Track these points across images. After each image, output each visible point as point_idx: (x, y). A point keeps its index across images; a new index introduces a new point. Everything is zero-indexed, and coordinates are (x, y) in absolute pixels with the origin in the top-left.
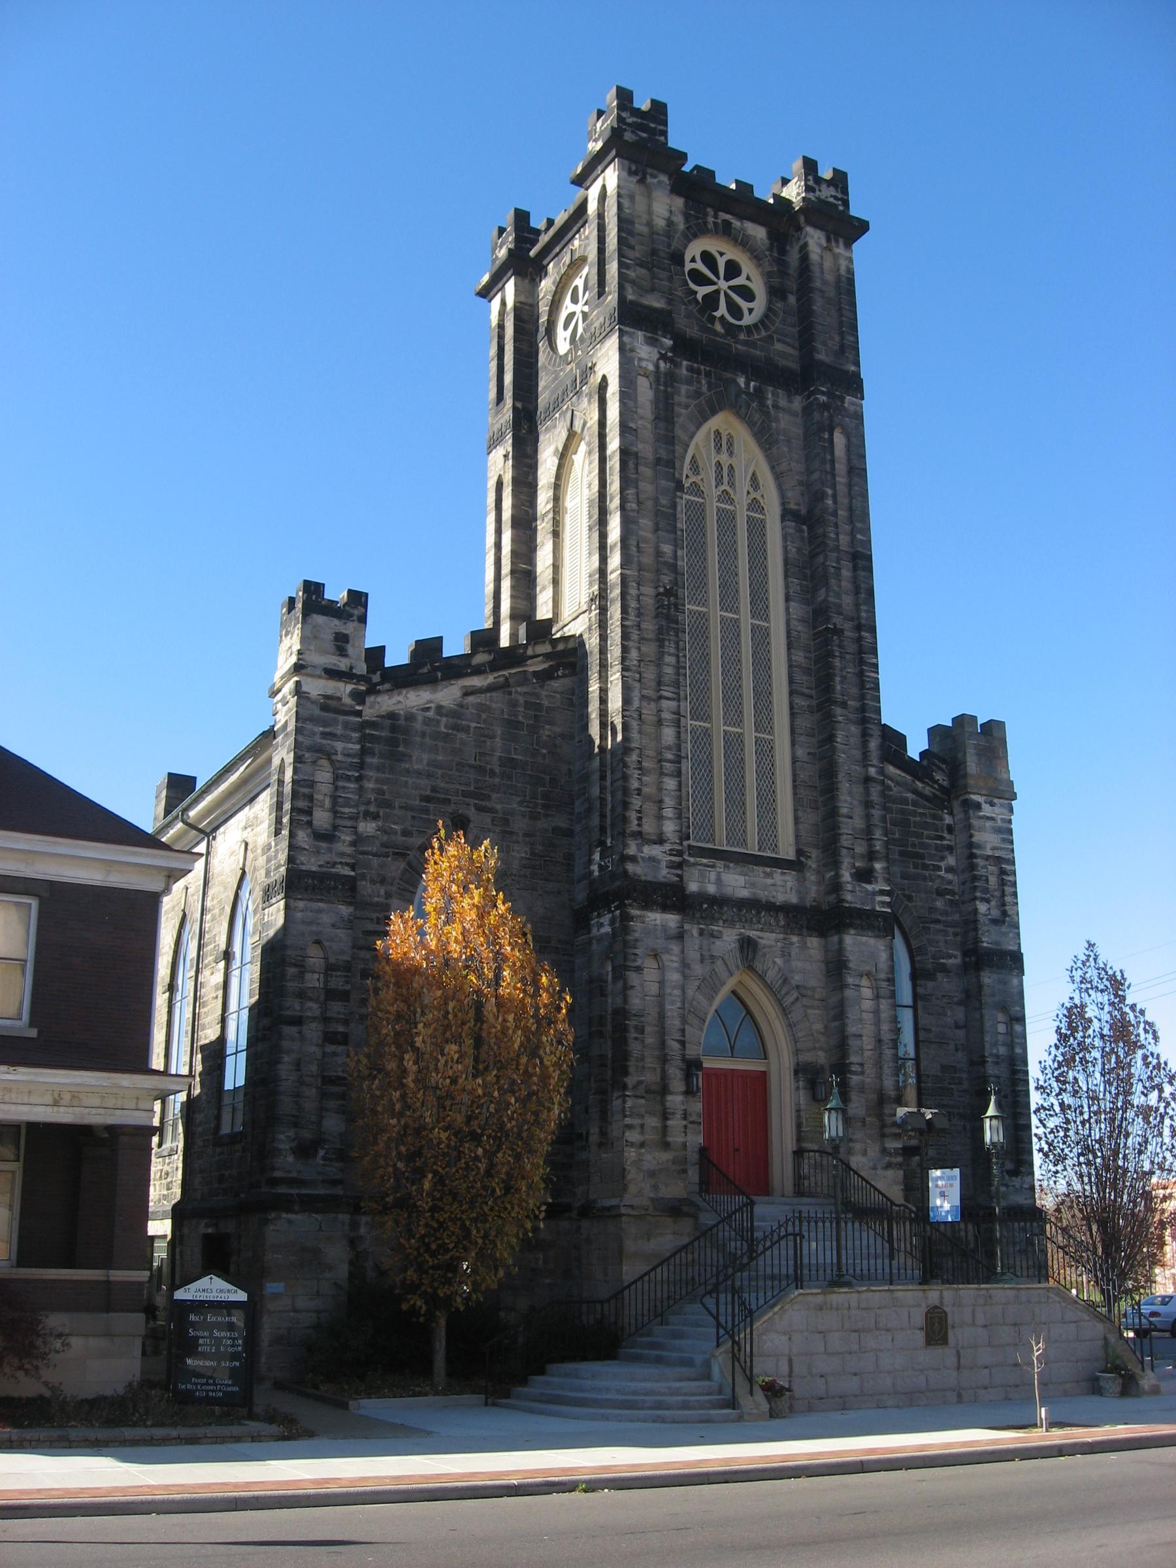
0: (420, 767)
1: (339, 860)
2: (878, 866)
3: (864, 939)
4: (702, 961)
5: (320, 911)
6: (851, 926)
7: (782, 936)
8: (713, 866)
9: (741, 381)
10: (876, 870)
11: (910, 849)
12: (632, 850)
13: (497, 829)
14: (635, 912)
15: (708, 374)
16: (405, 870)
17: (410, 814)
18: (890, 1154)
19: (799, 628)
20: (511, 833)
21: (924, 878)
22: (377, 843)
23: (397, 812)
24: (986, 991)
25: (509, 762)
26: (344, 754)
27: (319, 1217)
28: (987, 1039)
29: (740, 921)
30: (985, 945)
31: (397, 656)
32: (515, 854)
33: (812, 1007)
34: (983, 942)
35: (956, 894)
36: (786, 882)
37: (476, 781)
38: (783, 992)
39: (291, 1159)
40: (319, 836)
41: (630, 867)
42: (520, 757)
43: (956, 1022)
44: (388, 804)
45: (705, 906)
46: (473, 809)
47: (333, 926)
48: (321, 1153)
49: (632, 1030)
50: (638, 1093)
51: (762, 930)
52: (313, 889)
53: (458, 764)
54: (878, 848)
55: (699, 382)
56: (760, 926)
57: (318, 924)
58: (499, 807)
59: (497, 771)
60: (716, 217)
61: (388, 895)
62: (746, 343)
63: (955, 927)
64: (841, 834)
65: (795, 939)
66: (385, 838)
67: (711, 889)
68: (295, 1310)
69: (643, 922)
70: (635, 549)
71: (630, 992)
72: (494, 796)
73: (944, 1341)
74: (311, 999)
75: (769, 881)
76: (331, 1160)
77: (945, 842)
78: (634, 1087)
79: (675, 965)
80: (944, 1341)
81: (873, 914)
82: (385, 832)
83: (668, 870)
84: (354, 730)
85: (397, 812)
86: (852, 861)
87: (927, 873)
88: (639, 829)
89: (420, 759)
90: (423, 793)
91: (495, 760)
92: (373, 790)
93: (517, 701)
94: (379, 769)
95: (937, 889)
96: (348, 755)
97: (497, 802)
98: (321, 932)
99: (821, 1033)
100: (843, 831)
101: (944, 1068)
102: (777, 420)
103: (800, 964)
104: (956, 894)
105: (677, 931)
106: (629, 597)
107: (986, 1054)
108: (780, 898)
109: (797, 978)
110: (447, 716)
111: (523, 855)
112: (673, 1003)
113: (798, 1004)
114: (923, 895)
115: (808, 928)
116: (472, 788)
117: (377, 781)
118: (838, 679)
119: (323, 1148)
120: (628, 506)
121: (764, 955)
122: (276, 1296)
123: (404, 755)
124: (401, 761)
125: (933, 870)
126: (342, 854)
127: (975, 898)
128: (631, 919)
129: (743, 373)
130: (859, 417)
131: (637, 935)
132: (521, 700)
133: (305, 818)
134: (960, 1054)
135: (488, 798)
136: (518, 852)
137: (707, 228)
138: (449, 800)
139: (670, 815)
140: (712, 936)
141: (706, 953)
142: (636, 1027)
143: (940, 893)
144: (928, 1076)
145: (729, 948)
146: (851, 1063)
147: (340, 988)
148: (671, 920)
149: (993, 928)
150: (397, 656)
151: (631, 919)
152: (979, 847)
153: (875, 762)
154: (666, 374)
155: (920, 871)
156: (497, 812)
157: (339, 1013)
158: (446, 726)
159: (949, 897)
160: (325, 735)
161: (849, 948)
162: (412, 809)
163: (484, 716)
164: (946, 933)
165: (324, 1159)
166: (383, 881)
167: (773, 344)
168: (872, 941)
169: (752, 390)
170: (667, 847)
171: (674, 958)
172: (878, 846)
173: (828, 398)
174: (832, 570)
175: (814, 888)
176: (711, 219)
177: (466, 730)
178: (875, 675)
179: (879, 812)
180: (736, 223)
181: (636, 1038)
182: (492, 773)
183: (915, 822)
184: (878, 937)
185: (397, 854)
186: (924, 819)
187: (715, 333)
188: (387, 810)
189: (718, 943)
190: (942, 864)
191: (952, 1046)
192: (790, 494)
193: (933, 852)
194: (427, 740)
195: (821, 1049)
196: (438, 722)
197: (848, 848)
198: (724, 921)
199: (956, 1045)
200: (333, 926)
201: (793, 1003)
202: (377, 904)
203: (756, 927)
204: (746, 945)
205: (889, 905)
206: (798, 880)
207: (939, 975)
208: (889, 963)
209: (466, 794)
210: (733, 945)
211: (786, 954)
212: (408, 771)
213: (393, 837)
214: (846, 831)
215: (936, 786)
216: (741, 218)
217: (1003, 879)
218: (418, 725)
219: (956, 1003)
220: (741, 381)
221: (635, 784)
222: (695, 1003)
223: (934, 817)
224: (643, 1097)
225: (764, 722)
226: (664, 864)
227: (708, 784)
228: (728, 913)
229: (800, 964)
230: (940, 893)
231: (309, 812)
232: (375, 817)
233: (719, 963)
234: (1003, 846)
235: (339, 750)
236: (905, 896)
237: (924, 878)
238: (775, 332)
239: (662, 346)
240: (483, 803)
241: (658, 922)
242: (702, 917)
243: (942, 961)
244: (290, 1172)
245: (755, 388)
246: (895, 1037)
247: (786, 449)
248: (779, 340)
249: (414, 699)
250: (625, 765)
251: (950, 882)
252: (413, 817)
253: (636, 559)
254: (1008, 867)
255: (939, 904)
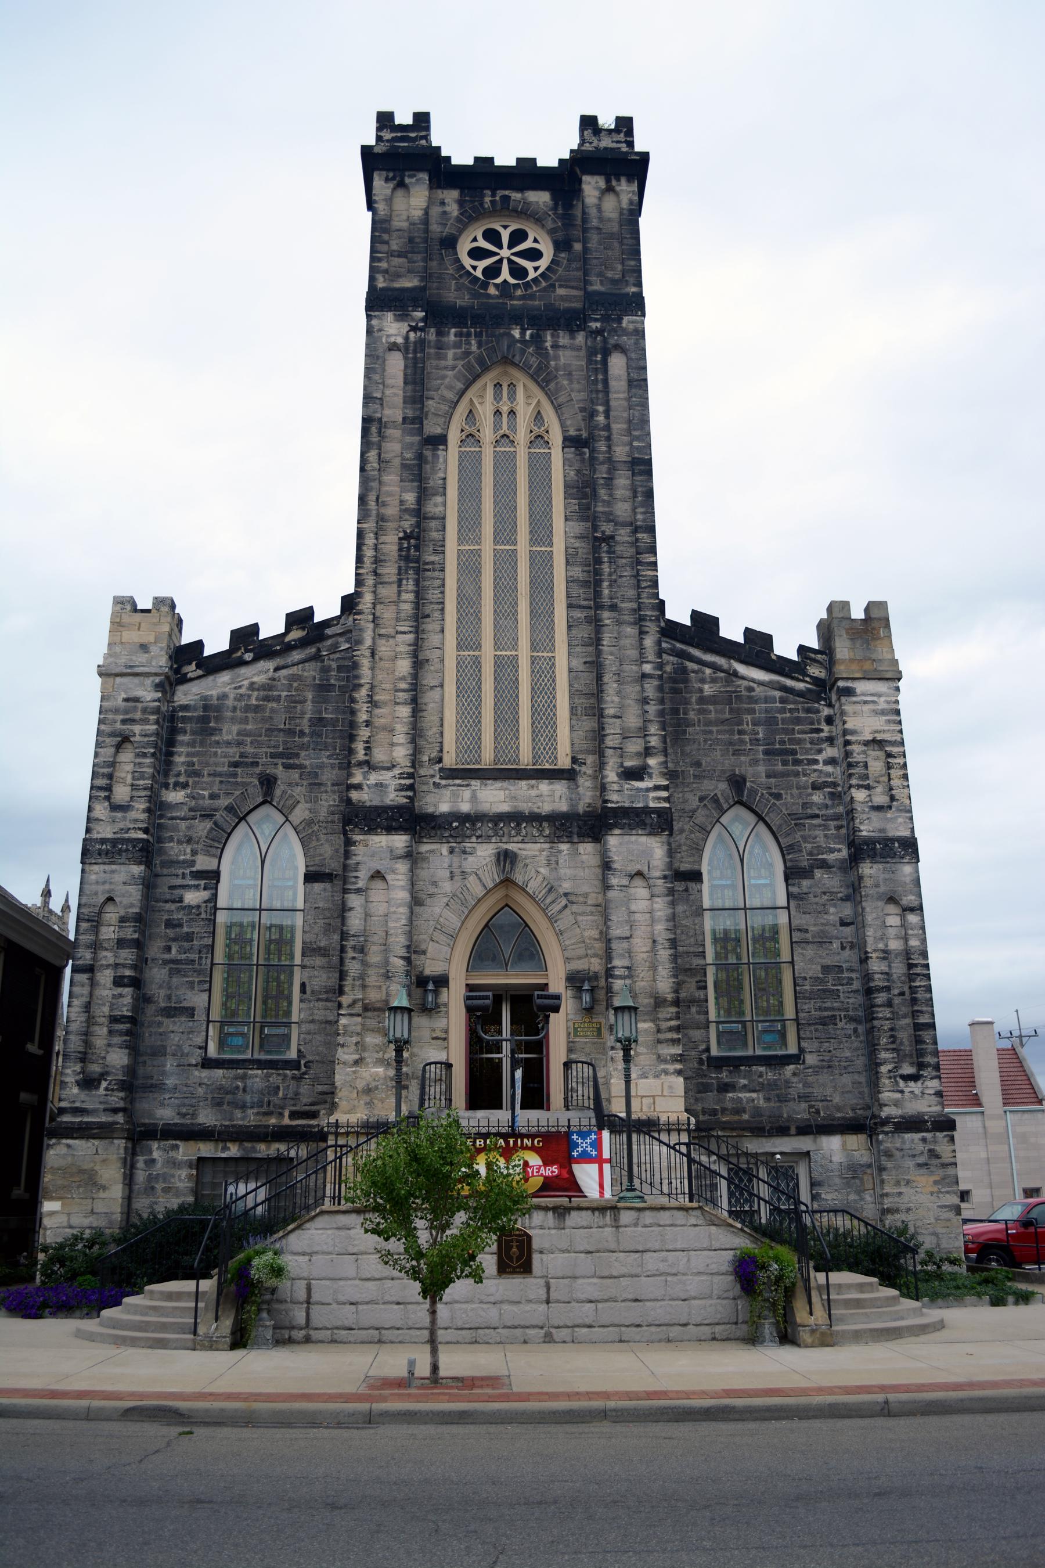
0: (230, 737)
1: (132, 826)
2: (652, 762)
3: (633, 838)
4: (452, 878)
5: (113, 872)
6: (615, 826)
7: (547, 845)
8: (467, 785)
9: (516, 333)
10: (649, 766)
11: (777, 746)
12: (357, 778)
13: (305, 783)
14: (357, 838)
15: (478, 335)
16: (212, 829)
17: (218, 779)
18: (665, 1061)
19: (577, 545)
20: (320, 784)
21: (797, 774)
22: (186, 808)
23: (206, 779)
24: (867, 882)
25: (318, 721)
26: (141, 735)
27: (96, 1142)
28: (868, 934)
29: (496, 835)
30: (864, 833)
31: (216, 644)
32: (323, 802)
33: (583, 914)
34: (861, 831)
35: (839, 785)
36: (553, 791)
37: (285, 743)
38: (548, 901)
39: (76, 1090)
40: (115, 808)
41: (354, 795)
42: (330, 716)
43: (841, 919)
44: (197, 774)
45: (455, 824)
46: (281, 768)
47: (124, 883)
48: (104, 1084)
49: (349, 950)
50: (353, 1012)
51: (523, 842)
52: (107, 854)
53: (268, 730)
54: (653, 744)
55: (469, 344)
56: (521, 838)
57: (111, 883)
58: (307, 763)
59: (307, 731)
60: (494, 195)
61: (194, 853)
62: (522, 298)
63: (837, 819)
64: (605, 735)
65: (564, 847)
66: (193, 803)
67: (465, 807)
68: (71, 1227)
69: (367, 845)
70: (374, 503)
71: (348, 914)
72: (303, 754)
73: (525, 1268)
74: (106, 949)
75: (534, 793)
76: (112, 1090)
77: (822, 735)
78: (349, 1006)
79: (401, 883)
80: (525, 1268)
81: (647, 811)
82: (194, 798)
83: (397, 793)
84: (153, 713)
85: (206, 779)
86: (619, 760)
87: (800, 769)
88: (367, 758)
89: (229, 731)
90: (232, 760)
91: (305, 722)
92: (183, 763)
93: (330, 666)
94: (192, 744)
95: (813, 783)
96: (145, 736)
97: (306, 759)
98: (113, 890)
99: (595, 939)
100: (608, 731)
101: (826, 969)
102: (557, 358)
103: (568, 872)
104: (839, 785)
105: (406, 850)
106: (365, 548)
107: (869, 950)
108: (546, 808)
109: (566, 886)
110: (258, 690)
111: (332, 803)
112: (397, 920)
113: (567, 911)
114: (795, 791)
115: (579, 835)
116: (281, 750)
117: (188, 755)
118: (606, 584)
119: (106, 1080)
120: (368, 467)
121: (526, 865)
122: (52, 1213)
123: (215, 729)
124: (212, 734)
125: (808, 764)
126: (136, 820)
127: (851, 786)
128: (354, 843)
129: (517, 324)
130: (640, 334)
131: (358, 858)
132: (334, 665)
133: (103, 794)
134: (847, 953)
135: (297, 756)
136: (326, 800)
137: (483, 208)
138: (257, 763)
139: (402, 741)
140: (464, 852)
141: (456, 870)
142: (354, 948)
143: (815, 787)
144: (805, 979)
145: (484, 863)
146: (614, 967)
147: (129, 937)
148: (400, 841)
149: (874, 815)
150: (216, 644)
151: (354, 843)
152: (853, 732)
153: (651, 658)
154: (415, 343)
155: (791, 768)
156: (305, 767)
157: (126, 959)
158: (257, 699)
159: (829, 790)
160: (124, 722)
161: (613, 849)
162: (220, 775)
163: (295, 684)
164: (826, 827)
165: (106, 1089)
166: (189, 841)
167: (554, 291)
168: (644, 839)
169: (527, 338)
170: (397, 771)
171: (400, 877)
172: (654, 741)
173: (602, 323)
174: (602, 481)
175: (589, 794)
176: (487, 199)
177: (278, 699)
178: (653, 573)
179: (654, 708)
180: (516, 196)
181: (354, 958)
182: (302, 733)
183: (783, 719)
184: (650, 834)
185: (204, 816)
186: (796, 714)
187: (489, 296)
188: (197, 779)
189: (471, 859)
190: (820, 758)
191: (836, 945)
192: (569, 422)
193: (809, 746)
194: (238, 713)
195: (595, 955)
196: (249, 696)
197: (615, 748)
198: (478, 837)
199: (842, 943)
200: (124, 883)
201: (560, 912)
202: (184, 862)
203: (516, 839)
204: (502, 858)
205: (667, 800)
206: (569, 788)
207: (818, 873)
208: (668, 860)
209: (273, 756)
210: (488, 859)
211: (552, 863)
212: (218, 743)
213: (201, 802)
214: (612, 731)
215: (808, 679)
216: (521, 189)
217: (888, 763)
218: (230, 702)
219: (842, 899)
220: (516, 333)
221: (363, 716)
222: (441, 920)
223: (808, 711)
224: (359, 1015)
225: (542, 640)
226: (392, 788)
227: (476, 708)
228: (486, 828)
229: (568, 872)
230: (815, 787)
231: (109, 788)
232: (185, 786)
233: (472, 878)
234: (886, 728)
235: (137, 732)
236: (771, 794)
237: (797, 774)
238: (556, 281)
239: (413, 319)
240: (291, 761)
241: (383, 844)
242: (451, 836)
243: (820, 857)
244: (74, 1102)
245: (532, 336)
246: (673, 936)
247: (565, 382)
248: (561, 286)
249: (222, 683)
250: (353, 700)
251: (829, 775)
252: (221, 782)
253: (374, 512)
254: (895, 750)
255: (817, 798)
